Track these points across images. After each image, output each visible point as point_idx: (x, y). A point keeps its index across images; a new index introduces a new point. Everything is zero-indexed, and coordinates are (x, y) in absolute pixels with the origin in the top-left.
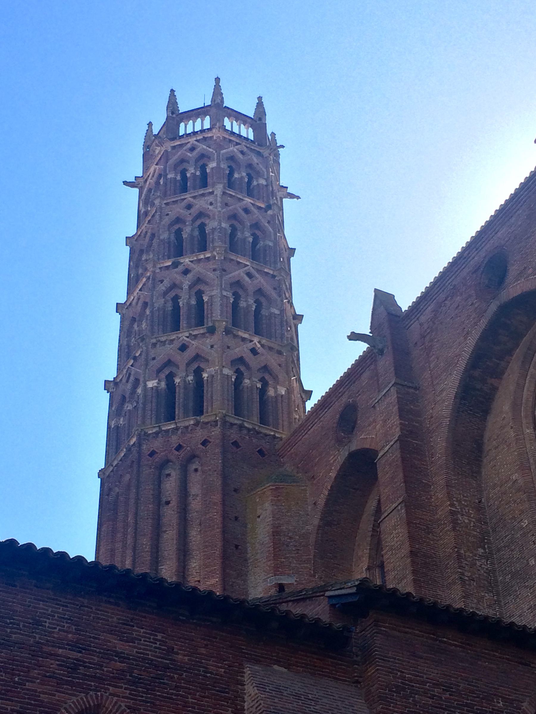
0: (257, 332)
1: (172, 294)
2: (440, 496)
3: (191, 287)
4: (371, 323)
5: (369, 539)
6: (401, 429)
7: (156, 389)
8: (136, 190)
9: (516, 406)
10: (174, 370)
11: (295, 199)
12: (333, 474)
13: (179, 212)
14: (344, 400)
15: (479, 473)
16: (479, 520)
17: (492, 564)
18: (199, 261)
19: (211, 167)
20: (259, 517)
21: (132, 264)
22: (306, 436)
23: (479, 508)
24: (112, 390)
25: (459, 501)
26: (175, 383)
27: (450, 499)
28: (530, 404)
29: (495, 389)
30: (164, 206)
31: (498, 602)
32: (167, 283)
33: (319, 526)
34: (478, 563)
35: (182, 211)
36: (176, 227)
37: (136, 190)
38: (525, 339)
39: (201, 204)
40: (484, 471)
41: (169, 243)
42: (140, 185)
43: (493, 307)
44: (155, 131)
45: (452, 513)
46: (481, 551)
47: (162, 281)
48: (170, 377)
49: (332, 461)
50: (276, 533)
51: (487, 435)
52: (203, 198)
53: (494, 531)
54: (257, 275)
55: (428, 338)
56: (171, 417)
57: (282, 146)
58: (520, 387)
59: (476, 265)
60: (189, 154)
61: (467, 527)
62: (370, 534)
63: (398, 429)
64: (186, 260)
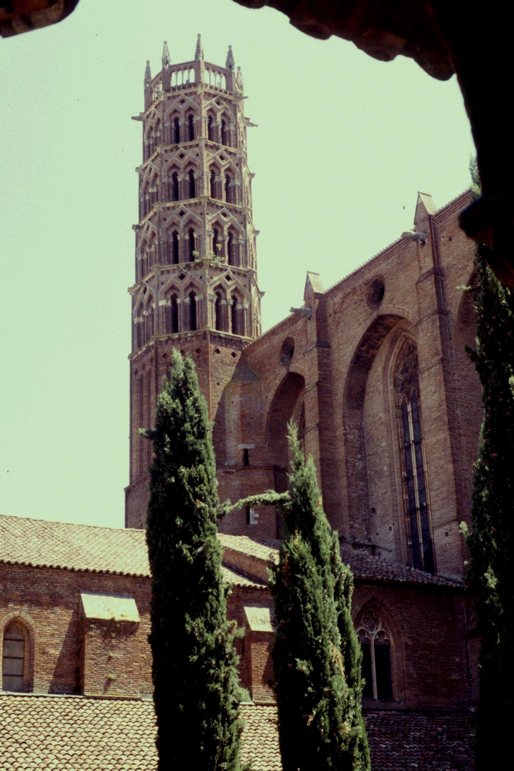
0: (224, 143)
1: (172, 230)
2: (339, 422)
3: (185, 226)
6: (319, 378)
7: (166, 308)
8: (141, 123)
9: (385, 369)
10: (176, 292)
11: (255, 127)
13: (175, 160)
15: (362, 405)
16: (360, 437)
17: (365, 463)
18: (190, 205)
20: (232, 403)
23: (361, 429)
25: (349, 426)
27: (344, 426)
28: (393, 370)
29: (374, 356)
30: (164, 152)
31: (366, 486)
32: (168, 220)
33: (269, 413)
34: (357, 464)
35: (177, 159)
36: (173, 171)
37: (141, 123)
38: (392, 330)
39: (190, 155)
40: (365, 405)
41: (169, 184)
43: (375, 315)
44: (153, 75)
45: (345, 435)
46: (359, 456)
47: (165, 220)
48: (174, 298)
50: (243, 416)
51: (368, 382)
52: (191, 149)
53: (368, 443)
54: (230, 214)
55: (337, 315)
56: (175, 329)
57: (246, 97)
58: (388, 359)
59: (367, 280)
60: (180, 106)
61: (352, 442)
63: (317, 377)
64: (182, 204)
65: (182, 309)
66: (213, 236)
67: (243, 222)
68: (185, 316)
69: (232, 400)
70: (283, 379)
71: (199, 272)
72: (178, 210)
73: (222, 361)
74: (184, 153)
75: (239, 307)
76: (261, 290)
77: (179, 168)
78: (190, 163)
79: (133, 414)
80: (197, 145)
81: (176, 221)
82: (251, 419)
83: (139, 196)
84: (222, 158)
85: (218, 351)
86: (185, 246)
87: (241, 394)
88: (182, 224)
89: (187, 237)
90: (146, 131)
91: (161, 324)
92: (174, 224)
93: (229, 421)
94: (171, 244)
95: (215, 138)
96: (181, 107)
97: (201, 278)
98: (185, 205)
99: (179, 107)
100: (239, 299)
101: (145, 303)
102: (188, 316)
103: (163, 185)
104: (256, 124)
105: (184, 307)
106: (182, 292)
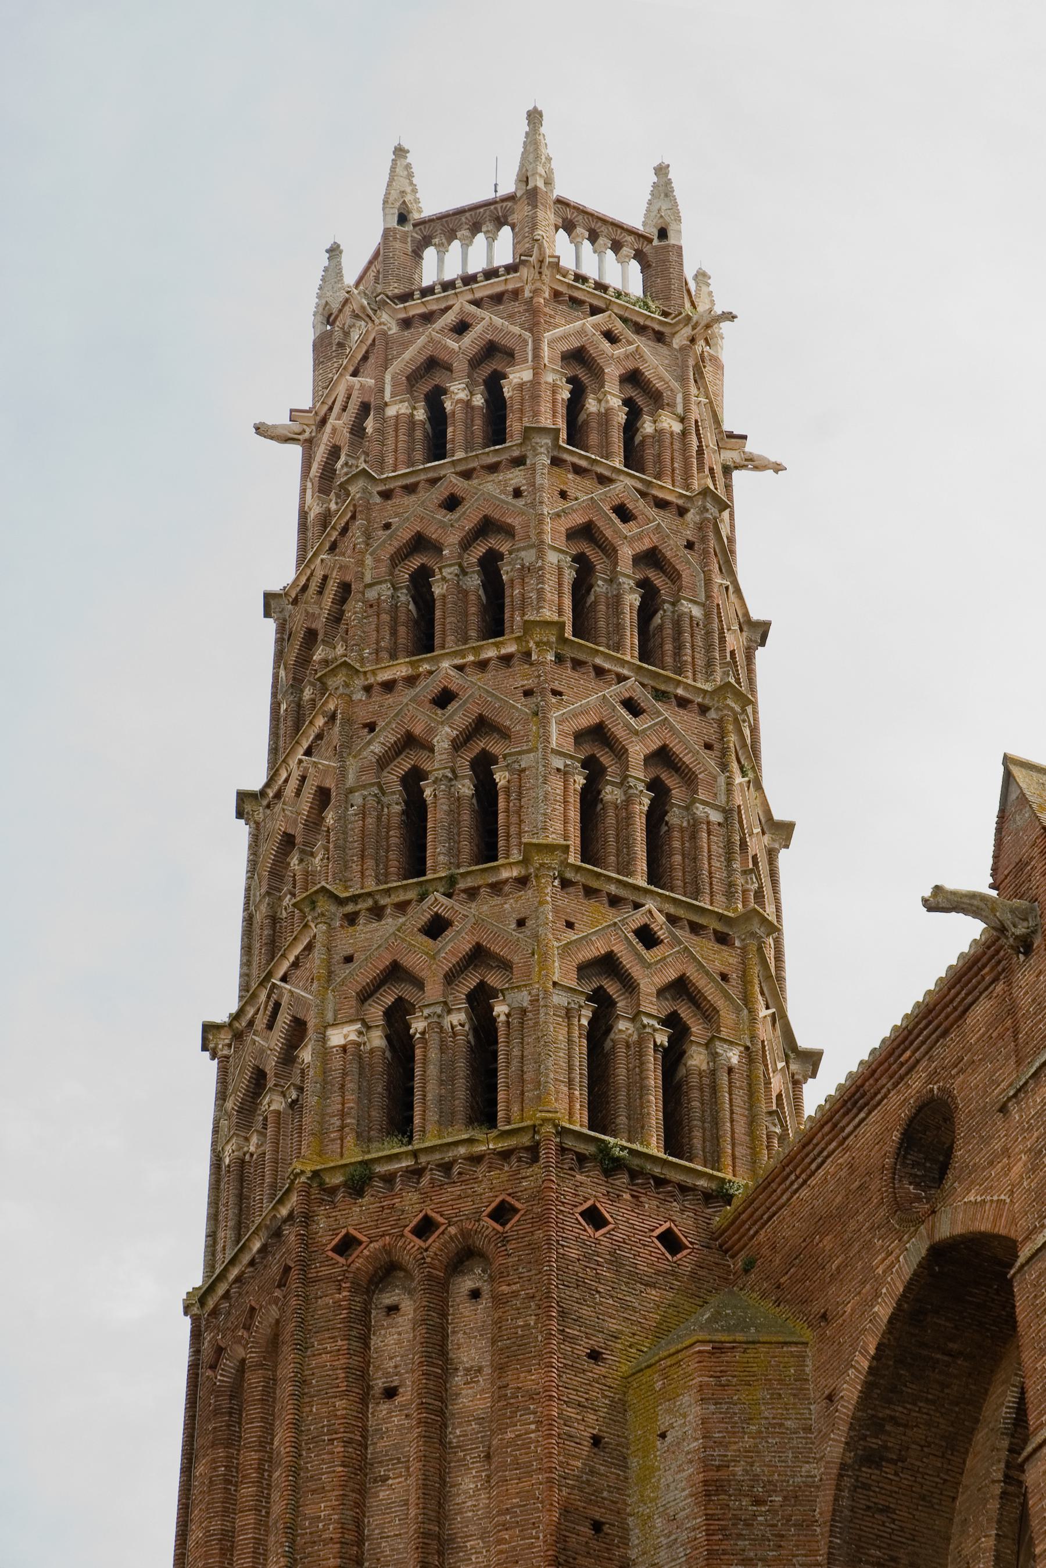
1: (404, 764)
3: (458, 745)
4: (996, 857)
5: (994, 1505)
8: (295, 452)
12: (883, 1310)
14: (917, 1084)
19: (516, 381)
20: (663, 1436)
21: (282, 673)
22: (804, 1193)
24: (226, 1052)
26: (412, 1031)
33: (843, 1466)
37: (295, 452)
42: (307, 435)
49: (880, 1271)
62: (997, 1489)
65: (433, 1054)
66: (579, 780)
67: (717, 746)
68: (447, 1080)
69: (664, 1421)
70: (908, 1288)
71: (512, 905)
72: (429, 688)
73: (615, 1261)
74: (460, 493)
75: (697, 1059)
76: (804, 1041)
77: (437, 548)
78: (487, 527)
79: (191, 1544)
80: (519, 462)
81: (418, 730)
82: (758, 1502)
83: (274, 695)
84: (624, 513)
85: (594, 1217)
86: (456, 822)
87: (701, 1387)
88: (442, 739)
89: (466, 788)
90: (315, 469)
91: (336, 1122)
92: (409, 742)
93: (646, 1520)
94: (395, 821)
95: (593, 438)
96: (454, 345)
97: (521, 923)
98: (460, 668)
99: (446, 347)
100: (697, 1029)
101: (270, 1065)
102: (461, 1083)
103: (370, 611)
104: (773, 458)
105: (443, 1048)
106: (434, 990)
